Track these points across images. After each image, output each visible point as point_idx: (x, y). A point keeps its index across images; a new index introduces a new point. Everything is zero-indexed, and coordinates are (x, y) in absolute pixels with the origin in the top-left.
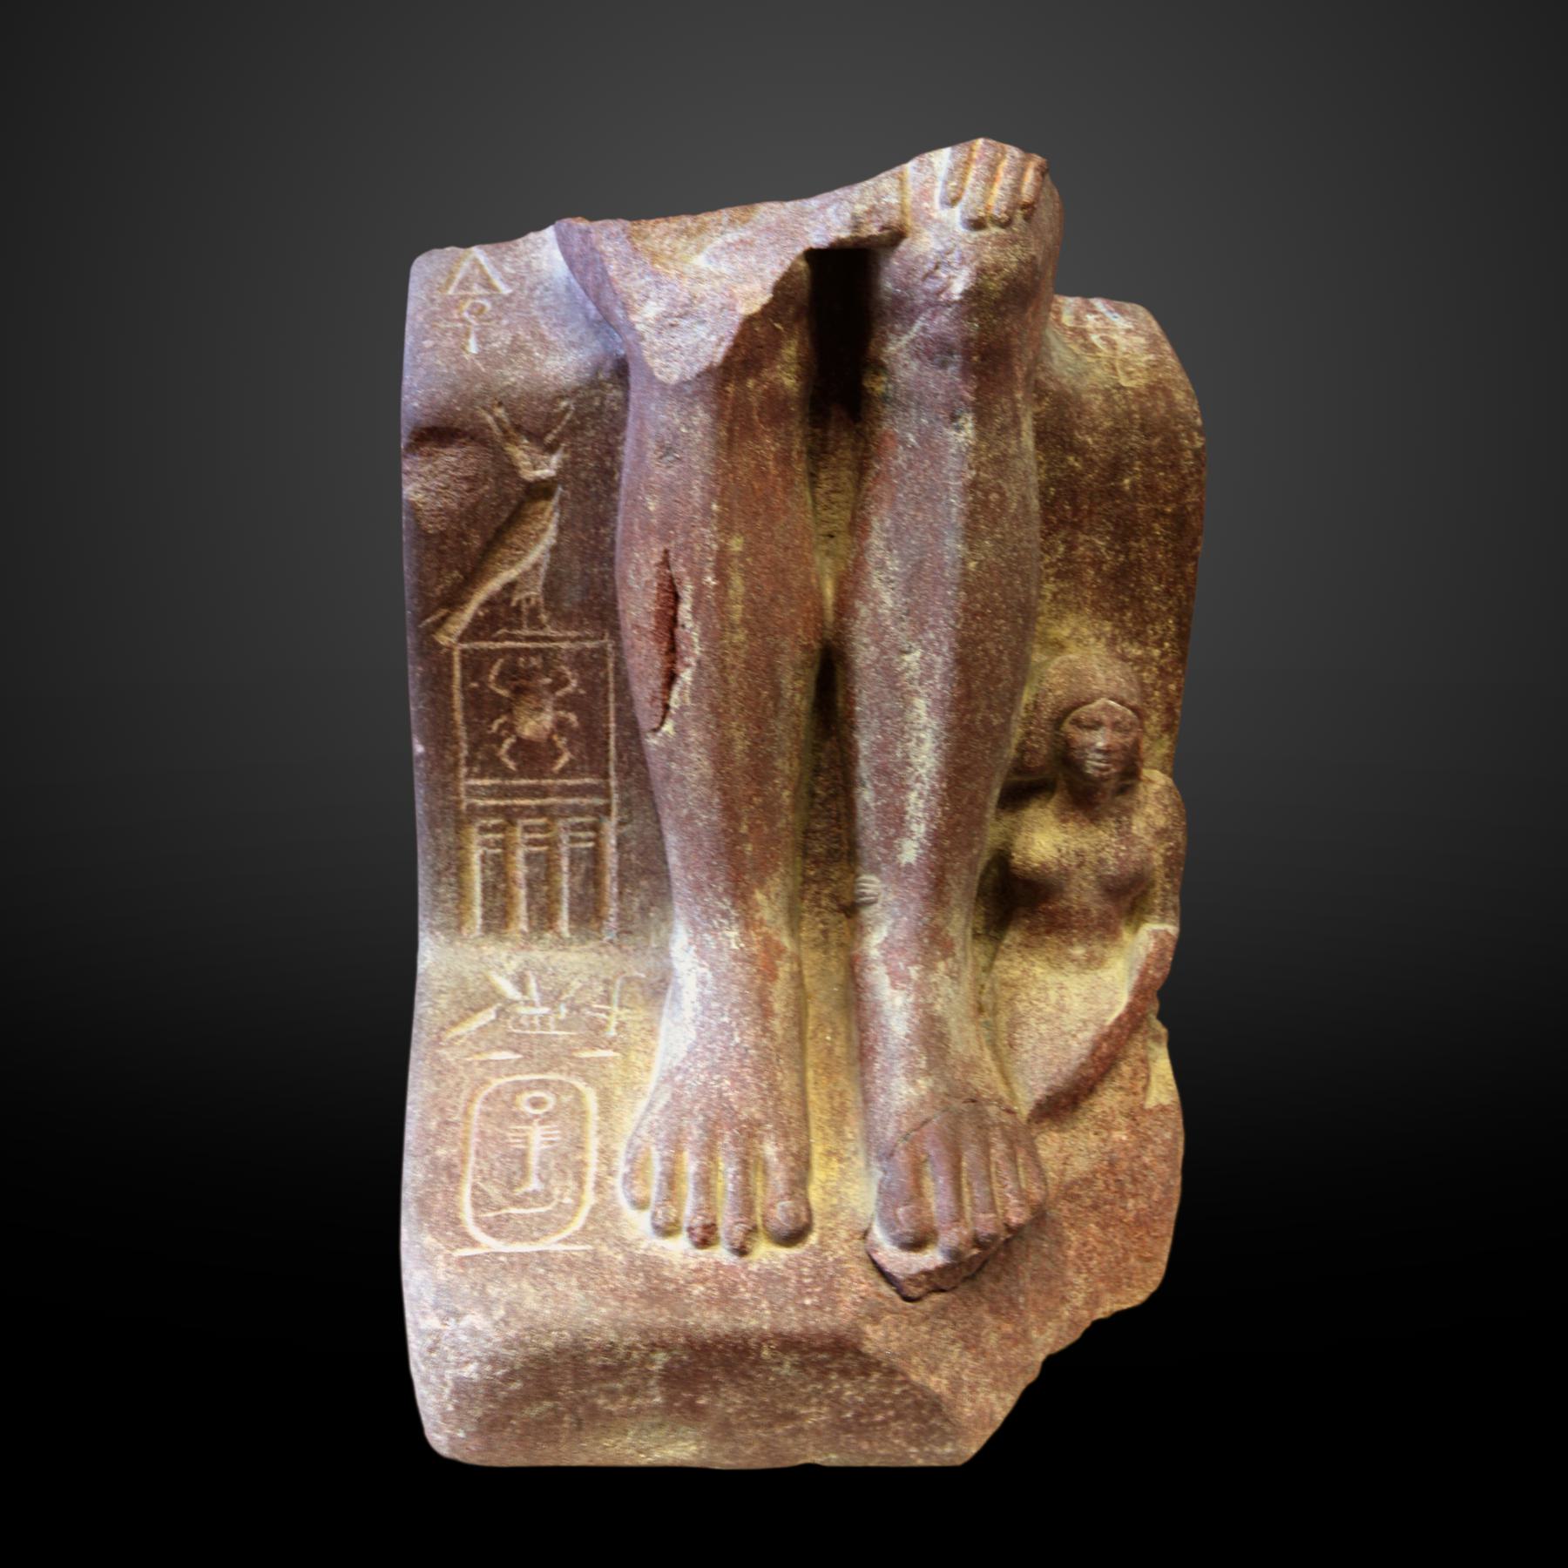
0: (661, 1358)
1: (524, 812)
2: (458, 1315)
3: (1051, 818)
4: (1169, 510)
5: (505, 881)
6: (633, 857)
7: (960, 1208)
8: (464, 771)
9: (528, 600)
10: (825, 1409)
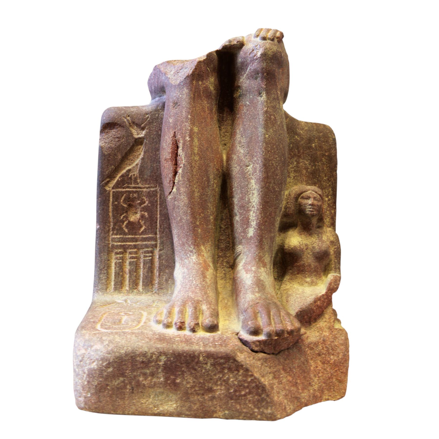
0: (163, 358)
1: (129, 247)
2: (91, 346)
3: (297, 234)
4: (327, 154)
5: (122, 272)
6: (164, 261)
7: (270, 322)
8: (111, 233)
9: (134, 175)
10: (223, 388)
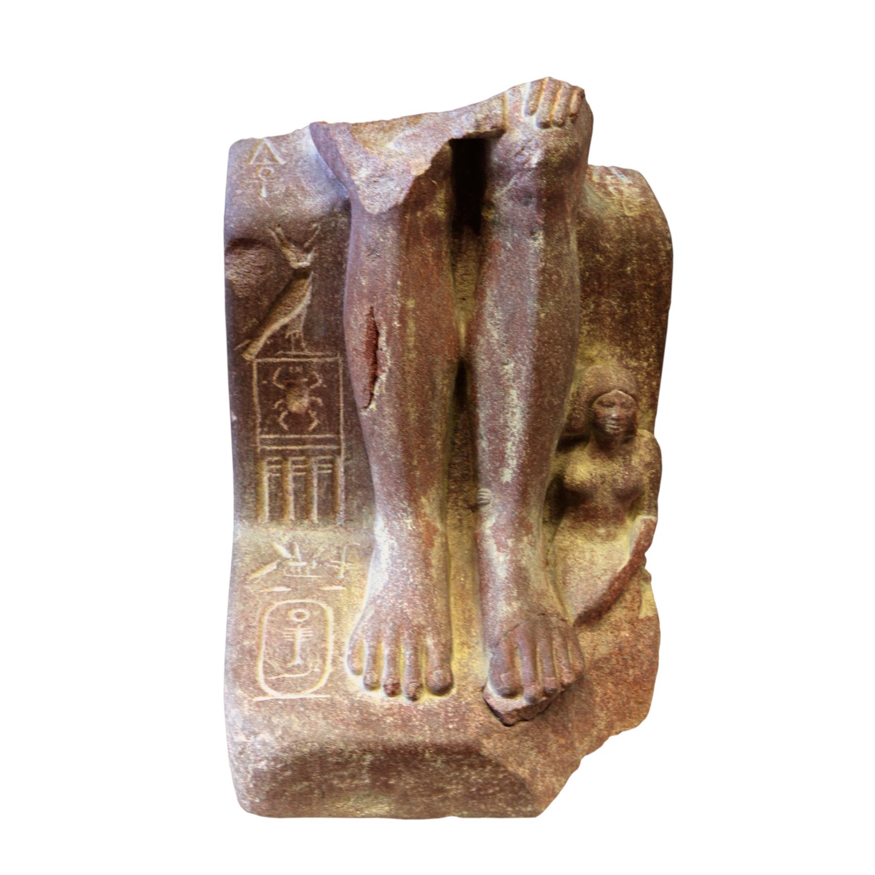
0: (369, 758)
1: (292, 453)
2: (256, 734)
3: (587, 456)
4: (652, 285)
5: (282, 491)
6: (353, 478)
7: (536, 674)
8: (259, 430)
9: (295, 335)
10: (460, 786)
